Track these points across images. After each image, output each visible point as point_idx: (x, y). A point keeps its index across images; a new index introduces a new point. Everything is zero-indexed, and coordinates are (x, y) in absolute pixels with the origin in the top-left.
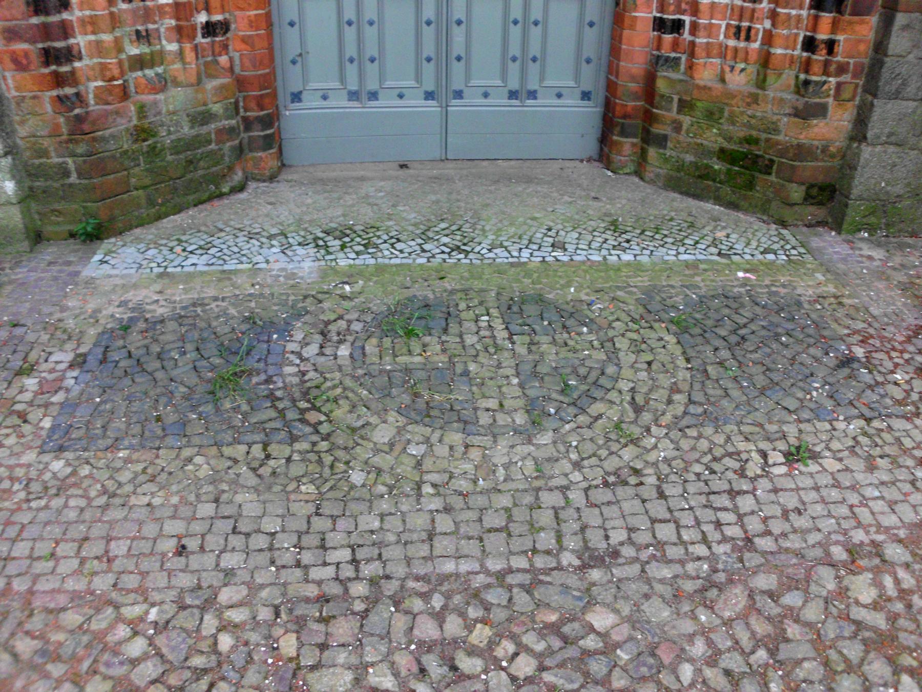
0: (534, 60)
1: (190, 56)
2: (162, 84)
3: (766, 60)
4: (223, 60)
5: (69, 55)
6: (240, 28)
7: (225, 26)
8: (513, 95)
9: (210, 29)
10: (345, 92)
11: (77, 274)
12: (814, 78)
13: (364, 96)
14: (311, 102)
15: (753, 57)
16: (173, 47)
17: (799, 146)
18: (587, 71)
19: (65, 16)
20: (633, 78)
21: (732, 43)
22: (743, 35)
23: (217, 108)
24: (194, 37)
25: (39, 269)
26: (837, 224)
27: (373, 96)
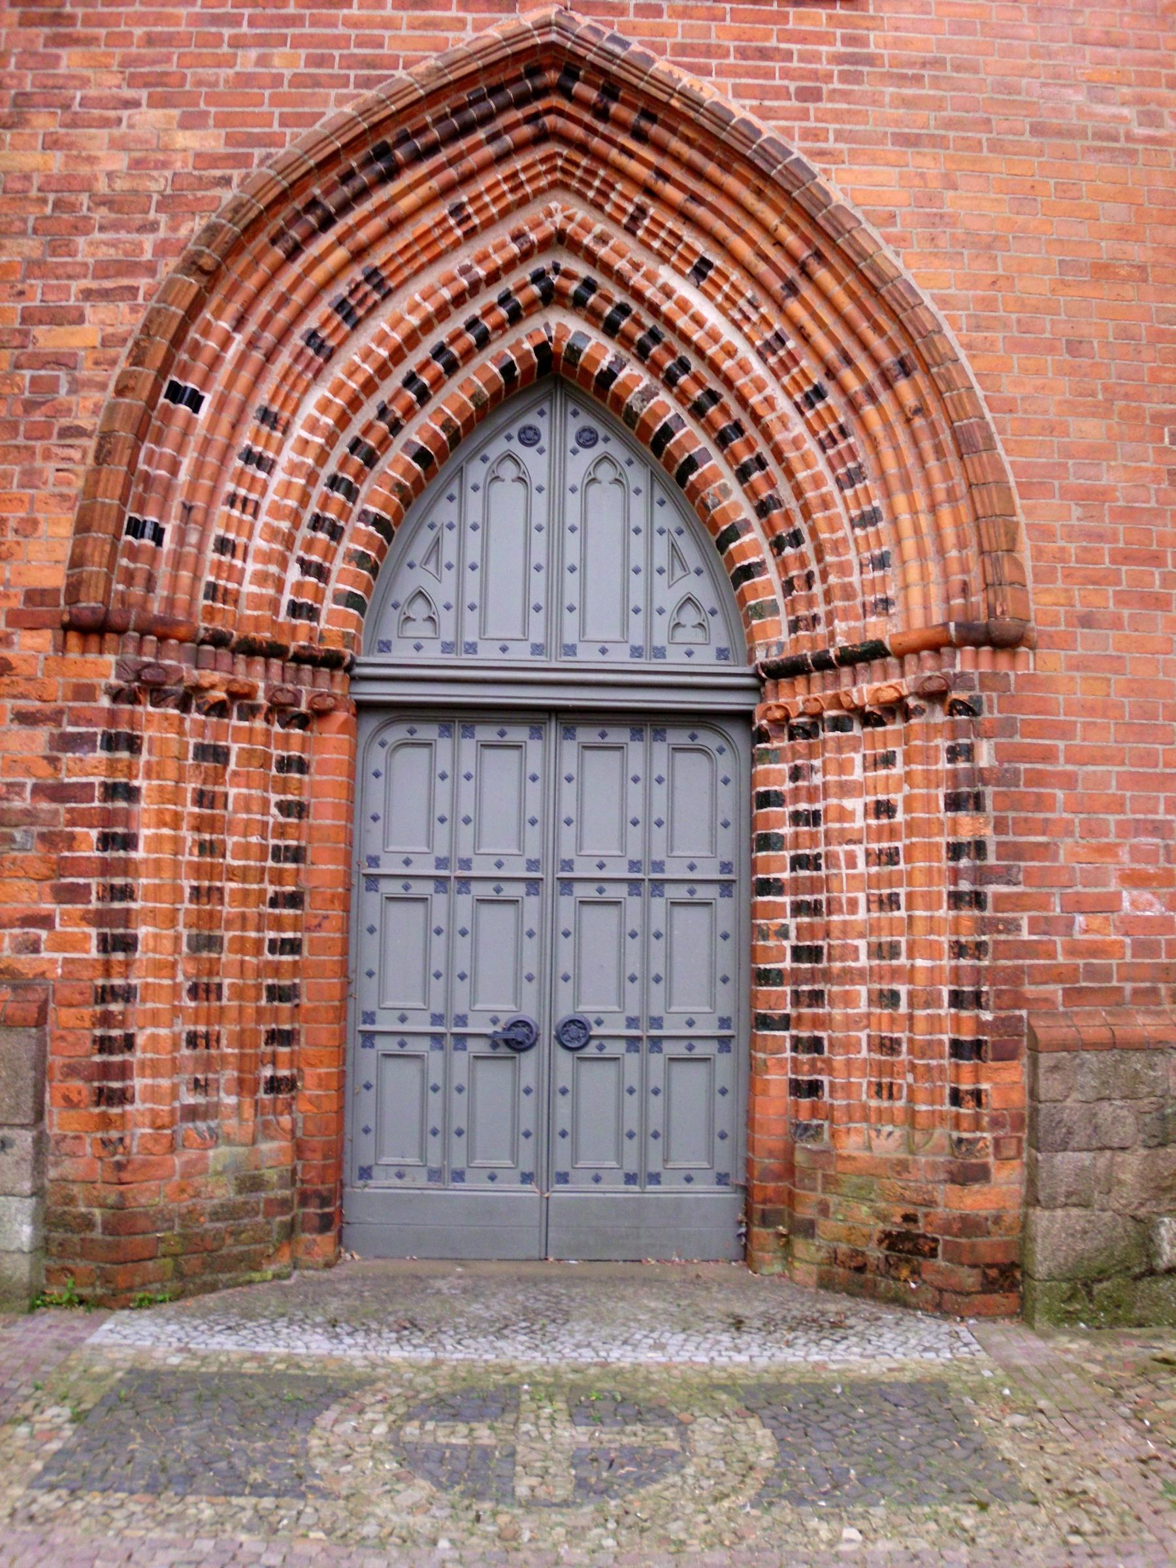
0: (656, 1135)
1: (248, 1112)
2: (215, 1138)
3: (911, 1116)
4: (286, 1120)
5: (123, 1097)
6: (310, 1089)
7: (290, 1084)
8: (630, 1179)
9: (274, 1085)
10: (424, 1171)
11: (82, 1339)
12: (965, 1135)
13: (447, 1175)
14: (382, 1182)
15: (899, 1116)
16: (231, 1100)
17: (964, 1219)
18: (722, 1148)
19: (127, 1057)
20: (771, 1154)
21: (874, 1103)
22: (885, 1093)
23: (272, 1175)
24: (255, 1091)
25: (41, 1332)
26: (1023, 1314)
27: (459, 1176)
